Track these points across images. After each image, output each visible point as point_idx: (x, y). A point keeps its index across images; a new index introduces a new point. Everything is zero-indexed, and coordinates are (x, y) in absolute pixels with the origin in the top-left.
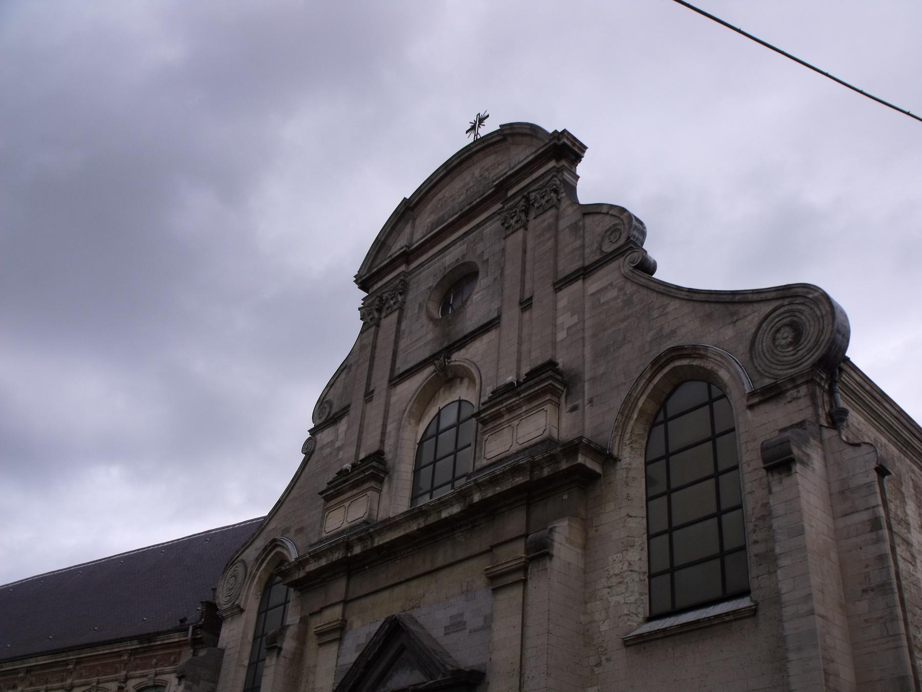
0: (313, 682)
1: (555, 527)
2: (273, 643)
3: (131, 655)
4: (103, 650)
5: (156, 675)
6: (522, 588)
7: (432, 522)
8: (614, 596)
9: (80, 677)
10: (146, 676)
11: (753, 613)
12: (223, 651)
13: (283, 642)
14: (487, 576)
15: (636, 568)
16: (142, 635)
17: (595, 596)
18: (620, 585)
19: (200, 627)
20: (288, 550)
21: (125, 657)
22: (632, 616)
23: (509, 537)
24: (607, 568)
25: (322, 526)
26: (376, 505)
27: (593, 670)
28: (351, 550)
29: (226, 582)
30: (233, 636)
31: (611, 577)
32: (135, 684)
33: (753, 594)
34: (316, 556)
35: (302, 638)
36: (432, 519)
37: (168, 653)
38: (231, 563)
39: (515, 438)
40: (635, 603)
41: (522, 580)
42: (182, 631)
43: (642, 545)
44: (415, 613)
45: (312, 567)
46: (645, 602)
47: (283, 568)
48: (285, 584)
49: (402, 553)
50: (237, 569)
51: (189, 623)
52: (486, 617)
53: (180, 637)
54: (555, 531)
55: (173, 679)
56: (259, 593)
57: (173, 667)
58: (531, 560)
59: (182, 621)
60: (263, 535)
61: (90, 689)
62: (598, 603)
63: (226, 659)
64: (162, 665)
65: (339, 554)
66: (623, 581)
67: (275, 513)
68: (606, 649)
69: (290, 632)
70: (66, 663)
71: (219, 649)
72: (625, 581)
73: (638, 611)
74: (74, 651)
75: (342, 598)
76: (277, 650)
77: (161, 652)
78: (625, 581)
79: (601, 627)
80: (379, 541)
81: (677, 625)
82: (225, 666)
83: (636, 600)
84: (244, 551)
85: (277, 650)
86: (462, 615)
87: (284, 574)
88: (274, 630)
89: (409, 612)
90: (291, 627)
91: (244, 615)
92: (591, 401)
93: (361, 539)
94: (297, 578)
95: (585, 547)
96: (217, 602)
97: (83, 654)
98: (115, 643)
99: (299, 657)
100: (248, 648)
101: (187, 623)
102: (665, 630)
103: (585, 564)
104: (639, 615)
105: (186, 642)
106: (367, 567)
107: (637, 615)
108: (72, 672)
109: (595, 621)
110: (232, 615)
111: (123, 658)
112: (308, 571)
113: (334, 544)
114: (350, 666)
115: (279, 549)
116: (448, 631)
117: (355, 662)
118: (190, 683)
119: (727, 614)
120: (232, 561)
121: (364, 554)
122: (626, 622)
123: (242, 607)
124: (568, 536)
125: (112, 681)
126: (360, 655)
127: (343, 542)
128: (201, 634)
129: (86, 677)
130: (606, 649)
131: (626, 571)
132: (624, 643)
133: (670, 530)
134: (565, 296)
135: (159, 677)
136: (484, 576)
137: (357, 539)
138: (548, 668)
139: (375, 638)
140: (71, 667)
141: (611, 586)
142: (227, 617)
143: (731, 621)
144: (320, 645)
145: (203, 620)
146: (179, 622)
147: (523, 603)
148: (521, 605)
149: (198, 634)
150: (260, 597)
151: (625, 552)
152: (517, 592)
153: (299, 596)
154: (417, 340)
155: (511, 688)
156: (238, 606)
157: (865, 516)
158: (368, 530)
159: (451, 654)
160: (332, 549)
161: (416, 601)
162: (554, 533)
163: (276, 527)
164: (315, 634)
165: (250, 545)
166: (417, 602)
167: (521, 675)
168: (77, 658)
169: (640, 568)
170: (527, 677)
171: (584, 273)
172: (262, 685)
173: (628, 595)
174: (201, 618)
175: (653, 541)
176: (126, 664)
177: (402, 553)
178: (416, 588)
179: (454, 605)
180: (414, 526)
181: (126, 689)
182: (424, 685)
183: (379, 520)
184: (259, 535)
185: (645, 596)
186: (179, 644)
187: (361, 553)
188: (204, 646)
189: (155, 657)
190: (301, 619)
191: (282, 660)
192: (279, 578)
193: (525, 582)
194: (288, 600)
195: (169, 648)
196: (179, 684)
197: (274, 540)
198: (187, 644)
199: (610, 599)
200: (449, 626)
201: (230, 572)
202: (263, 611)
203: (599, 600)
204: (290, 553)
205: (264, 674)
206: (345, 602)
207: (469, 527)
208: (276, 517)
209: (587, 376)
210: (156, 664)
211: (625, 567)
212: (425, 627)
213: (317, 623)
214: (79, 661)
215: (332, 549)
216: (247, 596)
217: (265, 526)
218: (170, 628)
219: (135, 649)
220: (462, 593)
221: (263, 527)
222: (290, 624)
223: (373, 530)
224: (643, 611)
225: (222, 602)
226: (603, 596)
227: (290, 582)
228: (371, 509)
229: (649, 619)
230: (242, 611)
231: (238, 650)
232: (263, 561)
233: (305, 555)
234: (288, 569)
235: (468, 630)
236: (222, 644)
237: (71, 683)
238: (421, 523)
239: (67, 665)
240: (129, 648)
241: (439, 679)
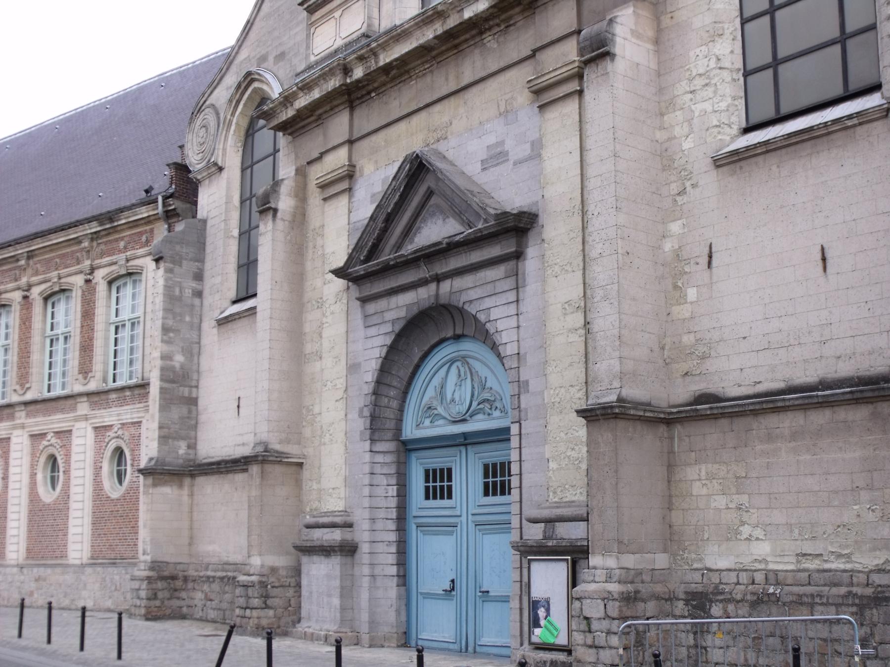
0: (323, 246)
1: (615, 17)
2: (265, 204)
3: (92, 240)
4: (57, 238)
5: (128, 260)
6: (577, 101)
7: (452, 25)
8: (698, 103)
9: (37, 273)
10: (115, 263)
11: (885, 113)
12: (204, 222)
13: (278, 201)
14: (531, 89)
15: (727, 64)
16: (101, 215)
17: (674, 105)
18: (706, 88)
19: (171, 196)
20: (268, 84)
21: (86, 244)
22: (723, 128)
23: (555, 36)
24: (687, 67)
25: (308, 47)
26: (376, 10)
27: (675, 201)
28: (350, 74)
29: (195, 135)
30: (214, 202)
31: (694, 78)
32: (104, 275)
33: (884, 88)
34: (306, 87)
35: (301, 195)
36: (452, 22)
37: (140, 232)
38: (198, 110)
40: (728, 110)
41: (576, 91)
42: (149, 204)
43: (734, 33)
44: (442, 147)
45: (302, 102)
46: (740, 108)
47: (265, 108)
48: (271, 129)
49: (417, 71)
50: (206, 117)
51: (156, 192)
52: (533, 144)
53: (148, 211)
54: (616, 23)
55: (148, 263)
56: (240, 144)
57: (147, 249)
58: (587, 63)
59: (147, 191)
60: (234, 68)
61: (52, 286)
62: (678, 113)
63: (210, 231)
64: (133, 248)
65: (335, 80)
66: (710, 82)
67: (245, 38)
68: (691, 173)
69: (285, 189)
70: (16, 259)
71: (200, 220)
72: (713, 82)
73: (732, 120)
74: (21, 243)
75: (346, 137)
76: (271, 212)
77: (128, 233)
78: (713, 82)
79: (683, 144)
80: (385, 59)
81: (783, 136)
82: (209, 240)
83: (728, 106)
84: (211, 93)
85: (271, 212)
86: (502, 143)
87: (267, 116)
88: (264, 188)
89: (434, 146)
90: (286, 182)
91: (225, 174)
93: (361, 58)
94: (284, 118)
95: (657, 42)
96: (187, 162)
97: (35, 245)
98: (70, 228)
99: (300, 218)
100: (235, 215)
101: (153, 193)
102: (766, 143)
103: (659, 63)
104: (733, 126)
105: (156, 217)
106: (373, 94)
107: (729, 126)
108: (25, 269)
109: (675, 138)
110: (210, 176)
111: (83, 245)
112: (297, 108)
113: (327, 69)
114: (366, 222)
115: (256, 85)
117: (372, 216)
118: (172, 266)
119: (850, 117)
120: (199, 107)
121: (369, 77)
122: (715, 136)
123: (220, 164)
124: (634, 28)
125: (76, 273)
126: (378, 206)
127: (338, 65)
128: (174, 204)
129: (44, 273)
130: (691, 173)
131: (714, 68)
132: (715, 163)
133: (776, 63)
135: (131, 263)
136: (527, 90)
137: (356, 58)
138: (617, 200)
139: (394, 183)
140: (22, 262)
141: (694, 91)
142: (204, 179)
143: (854, 126)
144: (325, 199)
145: (174, 187)
146: (144, 193)
147: (580, 121)
148: (578, 124)
149: (170, 205)
150: (241, 149)
151: (711, 43)
152: (571, 106)
153: (290, 142)
155: (571, 230)
156: (215, 164)
158: (368, 45)
159: (493, 195)
160: (325, 76)
161: (441, 130)
162: (615, 25)
163: (249, 56)
164: (318, 187)
165: (218, 84)
166: (443, 132)
167: (584, 213)
168: (28, 252)
169: (733, 63)
170: (591, 214)
172: (259, 258)
173: (717, 101)
174: (171, 184)
175: (748, 26)
176: (88, 251)
177: (417, 71)
178: (440, 115)
179: (490, 132)
180: (428, 33)
181: (94, 281)
182: (462, 236)
183: (382, 30)
184: (228, 69)
185: (739, 100)
186: (148, 221)
187: (363, 77)
188: (180, 218)
189: (122, 239)
190: (297, 170)
191: (279, 223)
192: (262, 122)
193: (580, 93)
194: (277, 148)
195: (137, 226)
196: (158, 268)
197: (249, 74)
198: (159, 219)
199: (693, 107)
200: (487, 159)
201: (198, 122)
202: (247, 167)
203: (679, 110)
204: (271, 88)
205: (259, 243)
206: (351, 142)
207: (502, 28)
208: (248, 43)
210: (125, 248)
211: (712, 64)
212: (456, 164)
213: (317, 173)
214: (30, 255)
215: (325, 76)
216: (224, 149)
217: (234, 58)
218: (134, 201)
219: (95, 233)
220: (500, 114)
221: (231, 58)
222: (284, 177)
223: (375, 44)
224: (738, 120)
225: (194, 161)
226: (684, 104)
227: (277, 125)
228: (369, 18)
229: (747, 130)
230: (221, 169)
231: (223, 218)
232: (238, 102)
233: (291, 88)
234: (271, 109)
235: (512, 162)
236: (201, 213)
237: (28, 282)
238: (439, 28)
239: (18, 260)
240: (89, 231)
241: (480, 226)
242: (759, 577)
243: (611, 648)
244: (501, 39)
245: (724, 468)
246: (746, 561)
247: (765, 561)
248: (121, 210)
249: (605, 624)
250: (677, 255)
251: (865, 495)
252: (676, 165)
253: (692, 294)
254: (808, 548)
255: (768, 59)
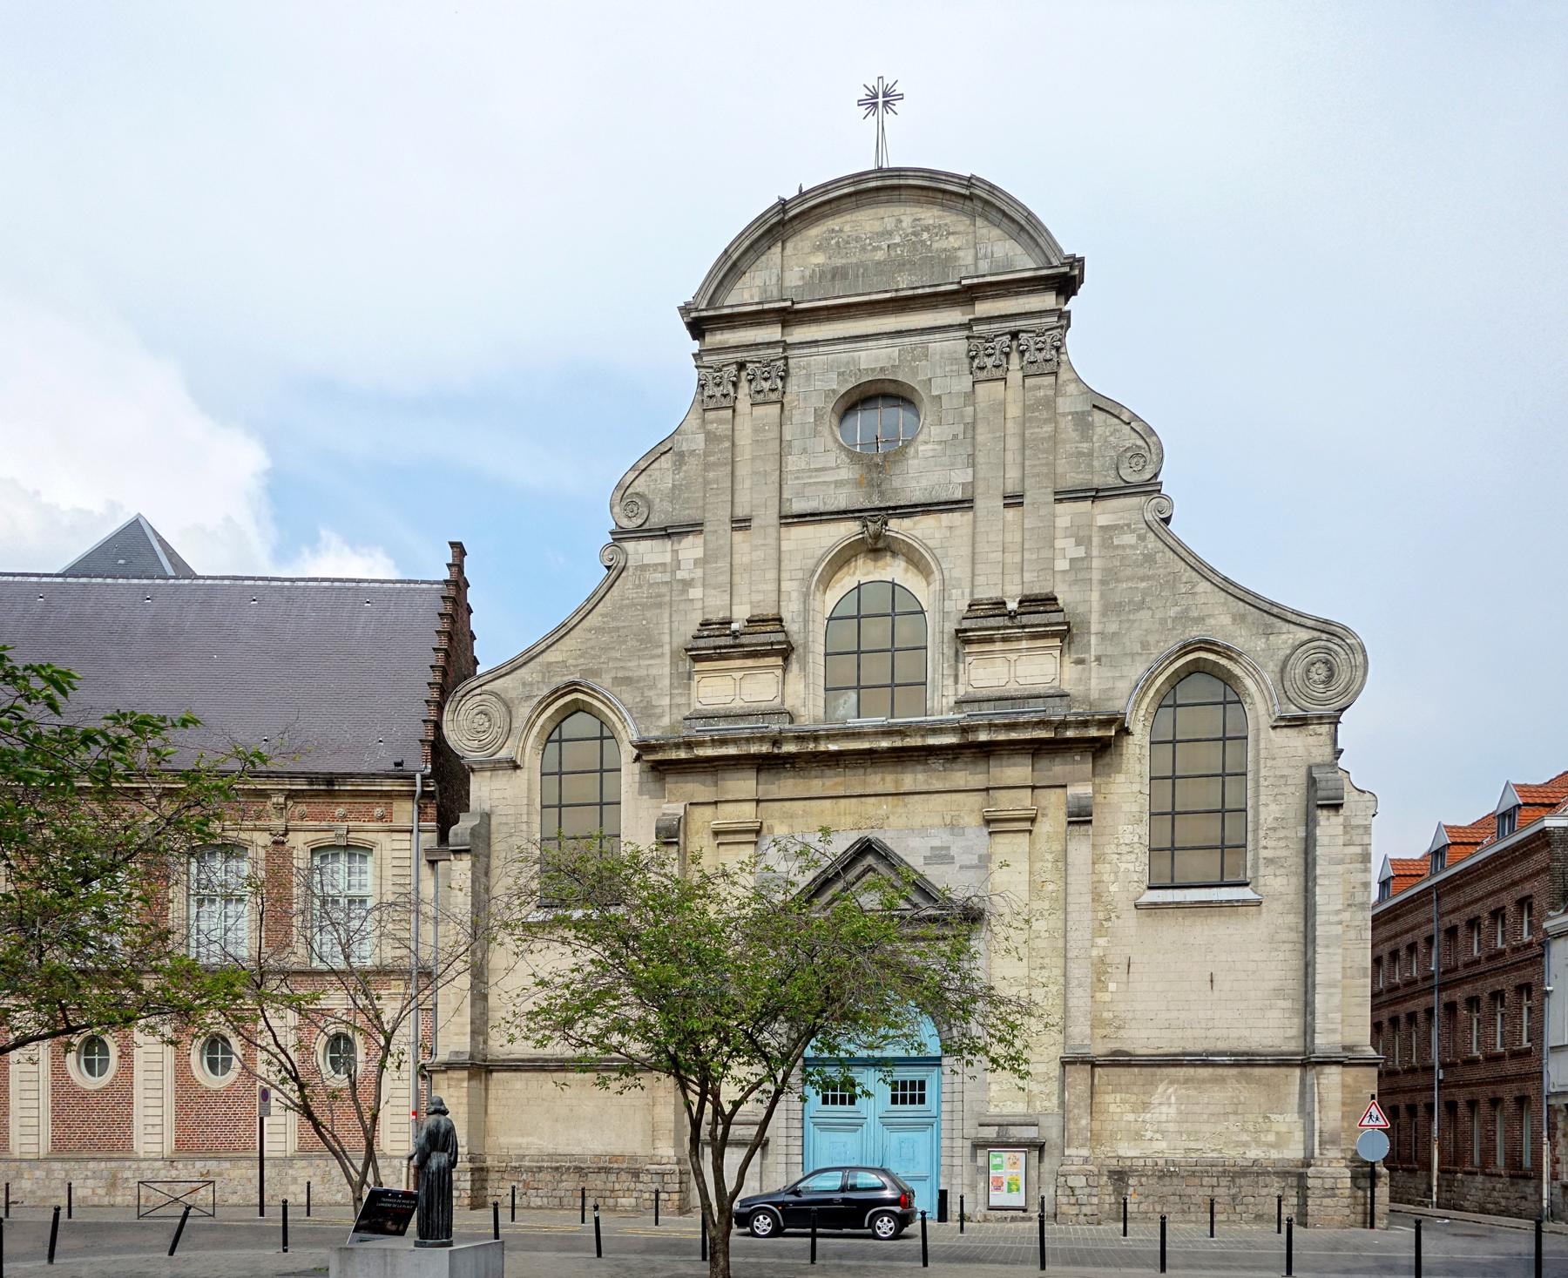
39: (1012, 675)
59: (397, 764)
92: (1098, 659)
116: (928, 860)
134: (1067, 513)
154: (817, 470)
157: (1358, 850)
171: (1097, 495)
209: (1094, 628)
240: (288, 787)
242: (1161, 1162)
243: (1091, 1204)
244: (947, 765)
245: (1134, 1096)
246: (1149, 1152)
247: (1163, 1152)
248: (351, 775)
249: (1087, 1190)
250: (1102, 960)
251: (1232, 1118)
252: (1103, 899)
253: (1112, 986)
254: (1193, 1145)
255: (557, 803)
